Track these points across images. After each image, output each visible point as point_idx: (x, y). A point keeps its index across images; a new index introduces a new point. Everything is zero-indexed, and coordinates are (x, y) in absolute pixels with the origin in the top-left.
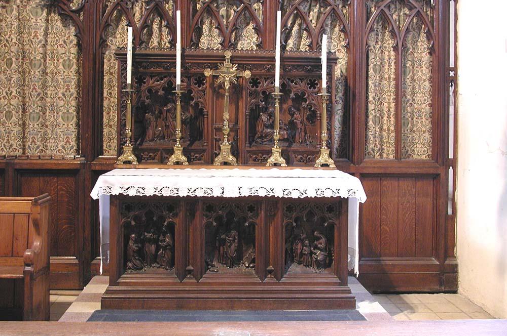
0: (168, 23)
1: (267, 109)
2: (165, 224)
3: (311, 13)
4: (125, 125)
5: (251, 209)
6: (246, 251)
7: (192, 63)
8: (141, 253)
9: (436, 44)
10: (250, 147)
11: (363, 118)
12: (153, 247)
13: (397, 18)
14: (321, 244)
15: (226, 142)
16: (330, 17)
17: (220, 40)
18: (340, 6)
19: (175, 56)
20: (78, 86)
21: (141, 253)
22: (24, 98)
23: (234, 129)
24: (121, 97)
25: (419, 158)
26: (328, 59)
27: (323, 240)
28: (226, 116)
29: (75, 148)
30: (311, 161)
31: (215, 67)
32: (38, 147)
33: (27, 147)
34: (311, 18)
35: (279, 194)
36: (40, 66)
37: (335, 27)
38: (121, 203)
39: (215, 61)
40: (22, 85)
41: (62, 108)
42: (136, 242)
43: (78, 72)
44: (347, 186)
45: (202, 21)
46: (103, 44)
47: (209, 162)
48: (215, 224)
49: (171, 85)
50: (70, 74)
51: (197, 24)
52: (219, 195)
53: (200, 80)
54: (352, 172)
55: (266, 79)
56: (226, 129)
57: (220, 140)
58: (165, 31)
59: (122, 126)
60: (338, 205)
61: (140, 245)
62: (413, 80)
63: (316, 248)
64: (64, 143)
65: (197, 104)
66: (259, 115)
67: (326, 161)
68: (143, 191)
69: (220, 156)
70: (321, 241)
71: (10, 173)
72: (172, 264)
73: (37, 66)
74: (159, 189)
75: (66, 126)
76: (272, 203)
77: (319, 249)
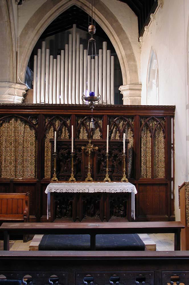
2: (69, 202)
3: (120, 124)
4: (54, 167)
9: (166, 135)
10: (98, 174)
13: (152, 125)
16: (127, 125)
17: (87, 134)
18: (131, 121)
19: (71, 142)
20: (35, 152)
22: (16, 156)
23: (92, 168)
24: (52, 157)
25: (161, 177)
26: (126, 142)
27: (123, 207)
30: (120, 179)
32: (21, 175)
33: (17, 175)
34: (120, 126)
36: (22, 145)
37: (129, 129)
38: (55, 195)
39: (85, 143)
40: (15, 151)
41: (30, 160)
42: (59, 208)
43: (35, 147)
44: (127, 187)
45: (80, 127)
46: (45, 137)
47: (83, 180)
50: (33, 147)
51: (78, 129)
52: (88, 192)
53: (80, 150)
55: (103, 150)
58: (67, 131)
59: (52, 167)
60: (128, 195)
61: (60, 210)
62: (158, 148)
63: (121, 210)
65: (79, 159)
67: (125, 179)
68: (62, 191)
69: (87, 178)
72: (71, 216)
73: (21, 145)
76: (105, 194)
77: (122, 210)
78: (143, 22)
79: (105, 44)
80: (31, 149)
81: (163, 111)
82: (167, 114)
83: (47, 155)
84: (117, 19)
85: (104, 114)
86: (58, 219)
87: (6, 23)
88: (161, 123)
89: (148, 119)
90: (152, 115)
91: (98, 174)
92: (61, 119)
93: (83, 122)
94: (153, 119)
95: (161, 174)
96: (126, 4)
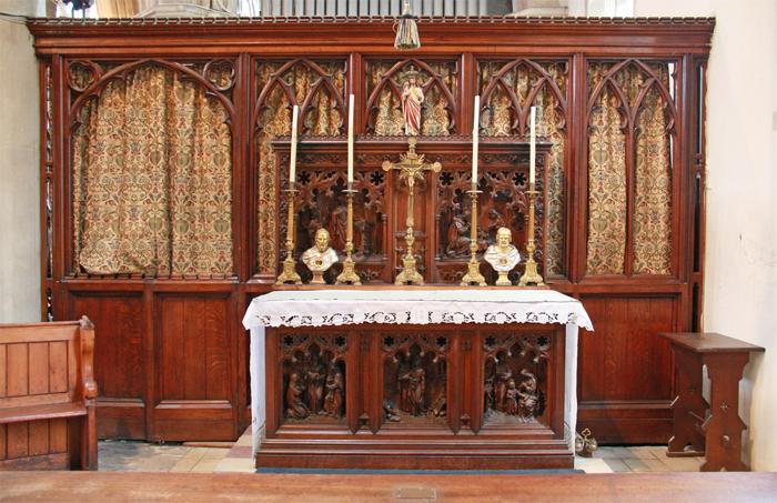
0: (338, 104)
1: (461, 212)
4: (285, 235)
6: (437, 393)
7: (368, 155)
8: (304, 396)
11: (583, 220)
12: (319, 391)
14: (530, 385)
16: (541, 92)
21: (304, 396)
28: (410, 221)
31: (396, 159)
32: (187, 265)
35: (480, 319)
37: (548, 104)
38: (281, 338)
39: (397, 151)
40: (168, 185)
42: (298, 382)
46: (258, 132)
48: (396, 361)
49: (342, 181)
53: (378, 178)
54: (569, 291)
55: (461, 173)
56: (410, 238)
57: (402, 253)
58: (335, 114)
60: (552, 334)
61: (303, 388)
63: (524, 390)
64: (217, 260)
66: (452, 221)
70: (530, 382)
71: (149, 297)
74: (329, 317)
76: (469, 330)
80: (217, 171)
81: (650, 40)
82: (684, 50)
85: (461, 49)
86: (293, 423)
89: (616, 68)
91: (441, 261)
92: (313, 69)
93: (388, 80)
95: (653, 259)
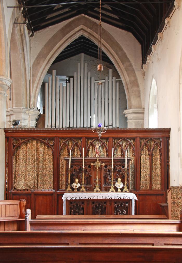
2: (81, 207)
4: (68, 180)
5: (105, 203)
15: (97, 185)
23: (100, 181)
29: (53, 187)
31: (94, 163)
32: (42, 187)
37: (131, 148)
40: (38, 168)
44: (132, 196)
48: (95, 207)
49: (81, 168)
53: (90, 166)
58: (79, 151)
60: (129, 201)
62: (155, 164)
65: (89, 173)
73: (42, 162)
75: (50, 181)
76: (111, 200)
78: (146, 52)
79: (111, 71)
81: (161, 133)
83: (62, 170)
84: (122, 48)
87: (21, 55)
88: (158, 144)
90: (150, 137)
92: (73, 140)
93: (92, 143)
94: (151, 140)
96: (131, 35)
